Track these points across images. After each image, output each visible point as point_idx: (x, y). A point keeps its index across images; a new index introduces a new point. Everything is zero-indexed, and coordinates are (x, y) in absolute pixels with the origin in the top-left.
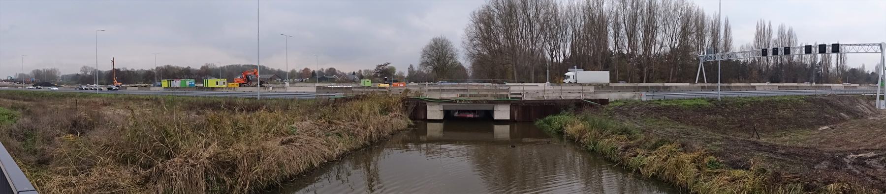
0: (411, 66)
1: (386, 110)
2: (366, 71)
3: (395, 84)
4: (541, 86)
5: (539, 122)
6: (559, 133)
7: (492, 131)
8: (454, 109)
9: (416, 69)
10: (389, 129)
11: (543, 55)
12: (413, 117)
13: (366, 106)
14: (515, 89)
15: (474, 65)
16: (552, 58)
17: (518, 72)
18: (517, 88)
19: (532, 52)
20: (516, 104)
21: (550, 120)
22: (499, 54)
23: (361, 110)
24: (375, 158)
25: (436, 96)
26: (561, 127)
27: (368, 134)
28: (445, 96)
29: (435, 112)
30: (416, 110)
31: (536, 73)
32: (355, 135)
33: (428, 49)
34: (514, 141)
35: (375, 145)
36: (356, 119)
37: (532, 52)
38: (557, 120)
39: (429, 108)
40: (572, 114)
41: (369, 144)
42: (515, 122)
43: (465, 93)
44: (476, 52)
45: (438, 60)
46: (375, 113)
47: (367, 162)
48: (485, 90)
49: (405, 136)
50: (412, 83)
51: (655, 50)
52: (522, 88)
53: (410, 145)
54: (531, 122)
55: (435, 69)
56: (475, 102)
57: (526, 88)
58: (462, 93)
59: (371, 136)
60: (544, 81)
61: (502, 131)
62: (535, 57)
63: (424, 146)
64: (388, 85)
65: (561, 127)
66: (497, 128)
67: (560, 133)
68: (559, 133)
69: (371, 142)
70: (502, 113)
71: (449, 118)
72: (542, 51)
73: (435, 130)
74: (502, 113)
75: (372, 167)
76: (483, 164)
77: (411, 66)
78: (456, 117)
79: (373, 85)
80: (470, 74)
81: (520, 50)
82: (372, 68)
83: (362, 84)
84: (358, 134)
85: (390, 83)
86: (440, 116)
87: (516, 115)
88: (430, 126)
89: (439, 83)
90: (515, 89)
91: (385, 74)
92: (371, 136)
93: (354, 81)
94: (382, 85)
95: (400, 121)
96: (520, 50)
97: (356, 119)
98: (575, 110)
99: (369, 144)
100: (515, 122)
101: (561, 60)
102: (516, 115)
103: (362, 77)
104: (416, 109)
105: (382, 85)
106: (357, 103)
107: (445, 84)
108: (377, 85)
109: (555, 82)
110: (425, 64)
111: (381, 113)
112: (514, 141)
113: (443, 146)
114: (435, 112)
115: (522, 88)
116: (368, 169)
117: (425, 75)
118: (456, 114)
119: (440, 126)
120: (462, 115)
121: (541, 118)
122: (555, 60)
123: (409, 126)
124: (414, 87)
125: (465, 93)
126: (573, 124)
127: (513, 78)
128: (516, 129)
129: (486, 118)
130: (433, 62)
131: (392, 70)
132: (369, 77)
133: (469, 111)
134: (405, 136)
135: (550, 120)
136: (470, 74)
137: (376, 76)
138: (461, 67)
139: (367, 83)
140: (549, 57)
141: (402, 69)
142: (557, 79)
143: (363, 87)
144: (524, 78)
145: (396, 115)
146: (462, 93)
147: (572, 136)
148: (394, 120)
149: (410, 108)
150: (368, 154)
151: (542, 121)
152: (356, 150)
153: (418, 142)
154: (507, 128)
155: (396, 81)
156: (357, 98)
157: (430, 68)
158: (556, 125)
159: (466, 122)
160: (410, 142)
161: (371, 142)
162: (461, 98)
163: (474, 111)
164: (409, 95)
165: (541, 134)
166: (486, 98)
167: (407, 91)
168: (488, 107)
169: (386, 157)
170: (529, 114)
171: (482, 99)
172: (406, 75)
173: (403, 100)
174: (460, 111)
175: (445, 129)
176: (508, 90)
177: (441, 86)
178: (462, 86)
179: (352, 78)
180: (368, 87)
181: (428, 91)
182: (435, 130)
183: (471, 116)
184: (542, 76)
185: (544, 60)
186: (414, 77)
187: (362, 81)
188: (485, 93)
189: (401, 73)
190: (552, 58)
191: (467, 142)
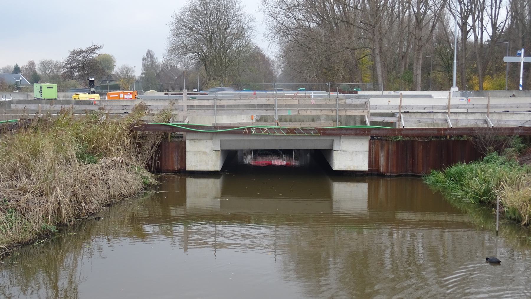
0: (150, 55)
1: (92, 152)
2: (45, 65)
3: (114, 94)
4: (439, 97)
5: (435, 178)
6: (482, 203)
7: (328, 195)
8: (245, 146)
9: (160, 59)
10: (99, 194)
11: (444, 27)
12: (156, 167)
13: (46, 142)
14: (383, 103)
15: (287, 53)
16: (465, 32)
17: (384, 66)
18: (383, 102)
19: (419, 21)
20: (383, 137)
21: (461, 174)
22: (342, 26)
23: (35, 153)
24: (69, 260)
25: (206, 120)
26: (487, 192)
27: (51, 206)
28: (225, 119)
29: (202, 155)
30: (160, 151)
31: (427, 69)
32: (22, 212)
33: (187, 18)
34: (380, 213)
35: (71, 227)
36: (21, 173)
37: (419, 21)
38: (478, 175)
39: (191, 147)
40: (515, 162)
41: (53, 228)
42: (381, 175)
43: (270, 113)
44: (291, 23)
45: (210, 41)
46: (68, 160)
47: (51, 269)
48: (311, 107)
49: (138, 208)
50: (152, 93)
51: (484, 40)
52: (395, 102)
53: (149, 229)
54: (416, 176)
55: (204, 60)
56: (291, 131)
57: (406, 102)
58: (262, 112)
59: (58, 211)
60: (445, 86)
61: (351, 197)
62: (425, 33)
63: (179, 228)
64: (96, 97)
65: (487, 192)
66: (340, 190)
67: (486, 203)
68: (482, 203)
69: (60, 225)
70: (352, 155)
71: (233, 166)
72: (439, 16)
73: (202, 194)
74: (352, 155)
75: (63, 283)
76: (309, 265)
77: (150, 55)
78: (249, 166)
79: (61, 96)
80: (279, 72)
81: (391, 16)
82: (60, 56)
83: (36, 94)
84: (28, 209)
85: (103, 90)
86: (214, 163)
87: (382, 160)
88: (192, 184)
89: (211, 93)
90: (383, 103)
91: (90, 71)
92: (58, 211)
93: (17, 87)
94: (83, 96)
95: (128, 175)
96: (391, 16)
97: (21, 173)
98: (521, 152)
99: (53, 228)
100: (381, 175)
101: (486, 38)
102: (382, 160)
103: (35, 79)
104: (161, 151)
105: (83, 96)
106: (26, 137)
107: (228, 95)
108: (72, 96)
109: (471, 88)
110: (179, 49)
111: (81, 158)
112: (380, 213)
113: (221, 228)
114: (202, 155)
115: (395, 102)
116: (55, 287)
117: (181, 75)
118: (249, 160)
119: (214, 185)
120: (261, 161)
121: (439, 167)
122: (471, 38)
123: (147, 186)
124: (156, 102)
125: (270, 113)
126: (516, 184)
127: (375, 79)
128: (382, 191)
129: (316, 168)
130: (197, 46)
131: (107, 62)
132: (53, 79)
133: (276, 153)
134: (138, 208)
135: (461, 174)
136: (279, 72)
137: (68, 76)
138: (258, 57)
139: (49, 91)
140: (458, 33)
141: (128, 60)
142: (476, 80)
143: (38, 101)
144: (400, 79)
145: (115, 163)
146: (262, 112)
147: (515, 210)
148: (112, 174)
149: (147, 146)
150: (52, 251)
151: (441, 175)
152: (23, 245)
153: (165, 220)
154: (361, 190)
155: (116, 88)
156: (24, 125)
157: (191, 60)
158: (476, 185)
159: (278, 175)
160: (152, 221)
161: (60, 225)
162: (261, 125)
163: (288, 153)
164: (145, 118)
165: (439, 203)
166: (315, 125)
167: (141, 108)
168: (319, 143)
169: (96, 253)
170: (415, 162)
171: (307, 125)
172: (138, 72)
173: (132, 129)
174: (258, 153)
175: (225, 192)
176: (365, 106)
177: (216, 98)
178: (262, 97)
179: (11, 80)
180: (51, 101)
181: (189, 110)
182: (202, 194)
183: (281, 162)
184: (439, 75)
185: (445, 38)
186: (156, 78)
187: (37, 86)
188: (314, 113)
189: (127, 70)
190: (465, 32)
191: (272, 219)
